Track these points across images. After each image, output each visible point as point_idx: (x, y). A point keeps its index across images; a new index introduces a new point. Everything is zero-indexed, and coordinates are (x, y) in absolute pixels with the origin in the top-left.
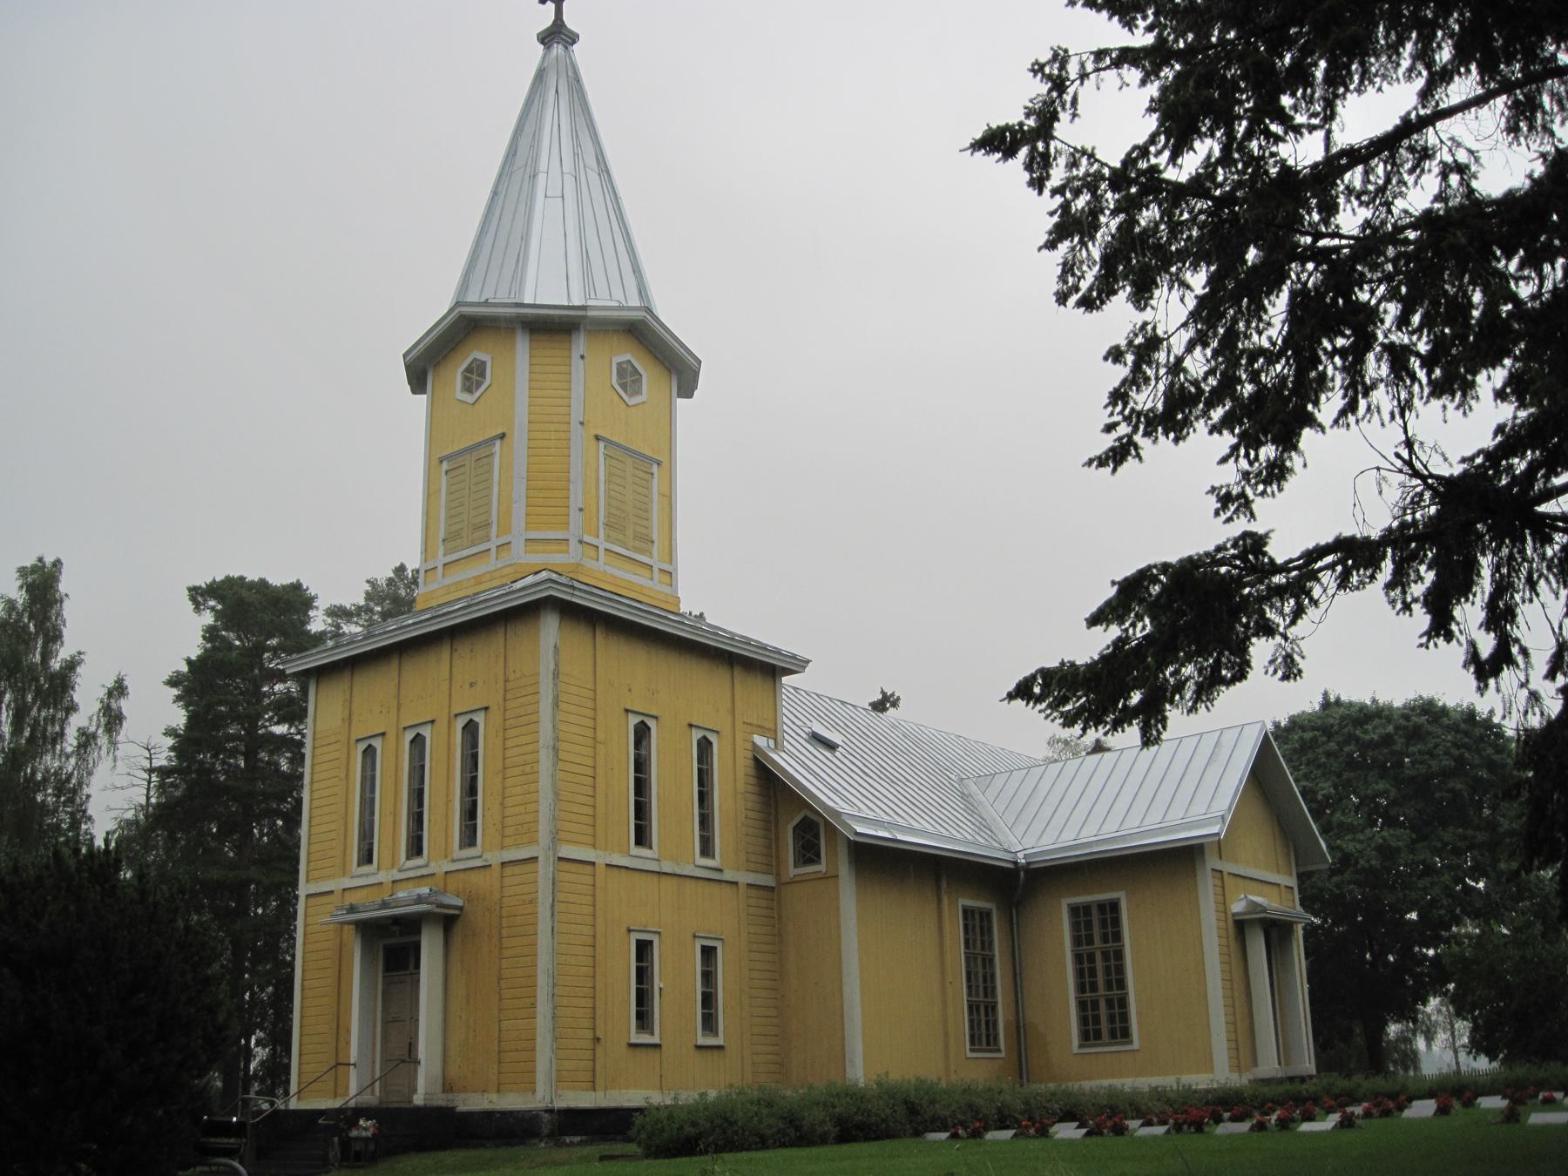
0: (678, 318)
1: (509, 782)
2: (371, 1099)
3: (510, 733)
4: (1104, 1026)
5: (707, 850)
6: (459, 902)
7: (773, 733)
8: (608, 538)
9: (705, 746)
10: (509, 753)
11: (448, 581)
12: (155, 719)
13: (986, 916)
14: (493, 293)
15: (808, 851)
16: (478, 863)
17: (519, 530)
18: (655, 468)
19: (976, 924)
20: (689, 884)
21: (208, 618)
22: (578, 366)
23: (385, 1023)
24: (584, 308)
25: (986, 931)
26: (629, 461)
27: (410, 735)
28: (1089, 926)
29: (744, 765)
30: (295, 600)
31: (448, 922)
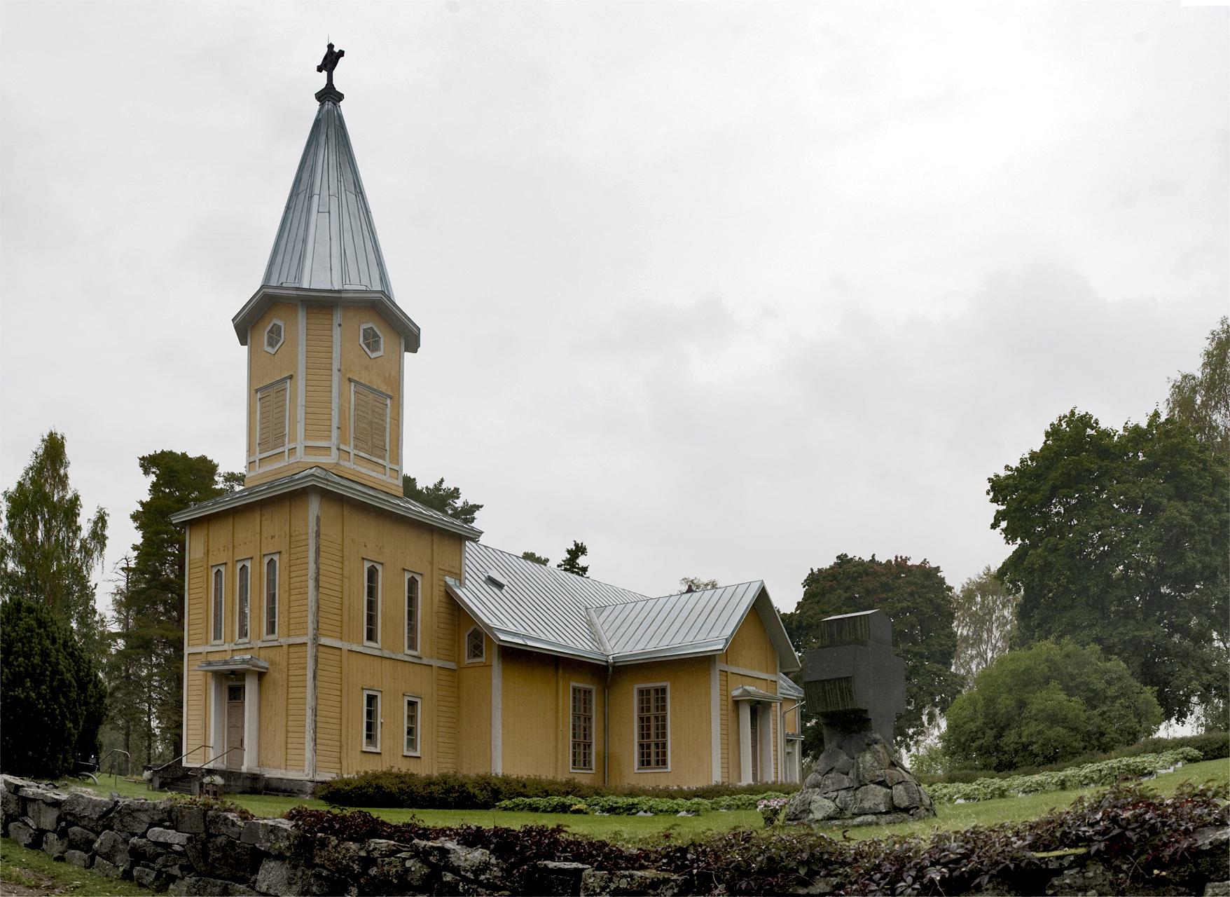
0: (406, 299)
1: (293, 598)
2: (221, 765)
3: (293, 569)
4: (653, 758)
5: (412, 646)
6: (266, 665)
7: (459, 577)
8: (356, 447)
9: (413, 583)
10: (293, 580)
11: (262, 470)
12: (124, 540)
13: (587, 692)
14: (286, 280)
15: (476, 650)
16: (276, 644)
17: (300, 443)
18: (388, 401)
19: (582, 698)
20: (400, 666)
21: (153, 478)
22: (337, 333)
23: (229, 727)
24: (339, 291)
25: (587, 701)
26: (371, 396)
27: (239, 566)
28: (649, 701)
29: (438, 594)
30: (204, 468)
31: (261, 676)
